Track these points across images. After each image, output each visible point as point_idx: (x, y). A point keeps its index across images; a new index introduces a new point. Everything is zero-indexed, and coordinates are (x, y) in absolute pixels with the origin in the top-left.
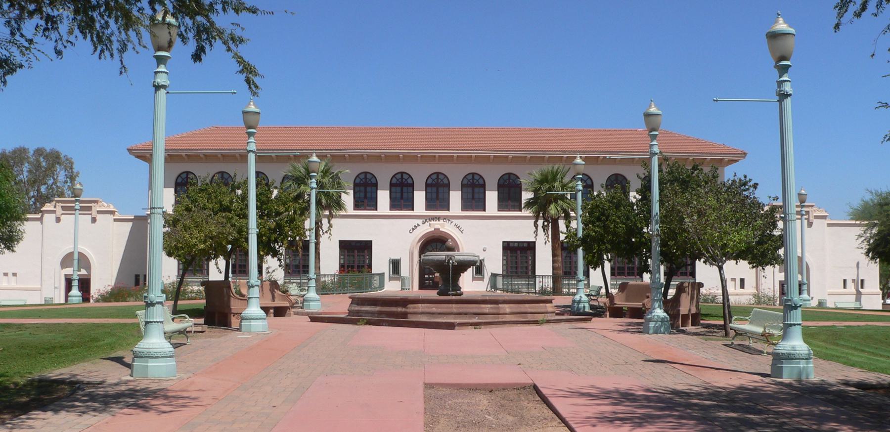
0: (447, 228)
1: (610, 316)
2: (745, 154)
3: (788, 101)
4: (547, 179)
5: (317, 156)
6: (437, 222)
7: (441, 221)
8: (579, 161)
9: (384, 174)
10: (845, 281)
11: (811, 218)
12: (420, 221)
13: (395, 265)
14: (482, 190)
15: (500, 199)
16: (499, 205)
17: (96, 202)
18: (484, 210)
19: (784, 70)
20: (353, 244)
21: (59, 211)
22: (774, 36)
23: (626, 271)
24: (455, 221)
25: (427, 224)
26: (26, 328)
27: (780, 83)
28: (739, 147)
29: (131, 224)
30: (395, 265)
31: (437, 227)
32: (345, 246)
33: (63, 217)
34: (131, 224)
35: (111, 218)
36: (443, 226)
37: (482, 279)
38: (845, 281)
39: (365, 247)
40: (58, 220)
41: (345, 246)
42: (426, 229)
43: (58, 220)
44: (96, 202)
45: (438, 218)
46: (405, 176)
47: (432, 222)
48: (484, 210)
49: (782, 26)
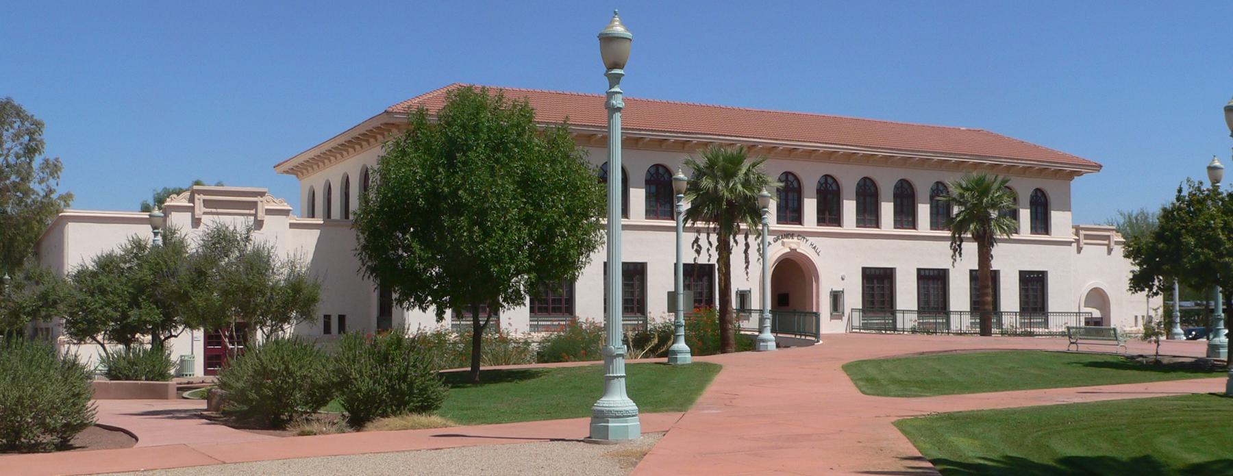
0: (803, 247)
2: (1101, 166)
3: (618, 116)
4: (981, 188)
11: (261, 215)
13: (836, 297)
15: (779, 209)
16: (895, 221)
17: (262, 194)
18: (878, 226)
19: (615, 80)
21: (200, 209)
22: (608, 40)
24: (811, 239)
27: (611, 95)
29: (317, 233)
30: (836, 297)
31: (794, 246)
34: (317, 233)
35: (286, 221)
36: (798, 244)
37: (840, 317)
40: (1079, 250)
42: (776, 251)
43: (1079, 250)
44: (262, 194)
48: (878, 226)
49: (619, 29)
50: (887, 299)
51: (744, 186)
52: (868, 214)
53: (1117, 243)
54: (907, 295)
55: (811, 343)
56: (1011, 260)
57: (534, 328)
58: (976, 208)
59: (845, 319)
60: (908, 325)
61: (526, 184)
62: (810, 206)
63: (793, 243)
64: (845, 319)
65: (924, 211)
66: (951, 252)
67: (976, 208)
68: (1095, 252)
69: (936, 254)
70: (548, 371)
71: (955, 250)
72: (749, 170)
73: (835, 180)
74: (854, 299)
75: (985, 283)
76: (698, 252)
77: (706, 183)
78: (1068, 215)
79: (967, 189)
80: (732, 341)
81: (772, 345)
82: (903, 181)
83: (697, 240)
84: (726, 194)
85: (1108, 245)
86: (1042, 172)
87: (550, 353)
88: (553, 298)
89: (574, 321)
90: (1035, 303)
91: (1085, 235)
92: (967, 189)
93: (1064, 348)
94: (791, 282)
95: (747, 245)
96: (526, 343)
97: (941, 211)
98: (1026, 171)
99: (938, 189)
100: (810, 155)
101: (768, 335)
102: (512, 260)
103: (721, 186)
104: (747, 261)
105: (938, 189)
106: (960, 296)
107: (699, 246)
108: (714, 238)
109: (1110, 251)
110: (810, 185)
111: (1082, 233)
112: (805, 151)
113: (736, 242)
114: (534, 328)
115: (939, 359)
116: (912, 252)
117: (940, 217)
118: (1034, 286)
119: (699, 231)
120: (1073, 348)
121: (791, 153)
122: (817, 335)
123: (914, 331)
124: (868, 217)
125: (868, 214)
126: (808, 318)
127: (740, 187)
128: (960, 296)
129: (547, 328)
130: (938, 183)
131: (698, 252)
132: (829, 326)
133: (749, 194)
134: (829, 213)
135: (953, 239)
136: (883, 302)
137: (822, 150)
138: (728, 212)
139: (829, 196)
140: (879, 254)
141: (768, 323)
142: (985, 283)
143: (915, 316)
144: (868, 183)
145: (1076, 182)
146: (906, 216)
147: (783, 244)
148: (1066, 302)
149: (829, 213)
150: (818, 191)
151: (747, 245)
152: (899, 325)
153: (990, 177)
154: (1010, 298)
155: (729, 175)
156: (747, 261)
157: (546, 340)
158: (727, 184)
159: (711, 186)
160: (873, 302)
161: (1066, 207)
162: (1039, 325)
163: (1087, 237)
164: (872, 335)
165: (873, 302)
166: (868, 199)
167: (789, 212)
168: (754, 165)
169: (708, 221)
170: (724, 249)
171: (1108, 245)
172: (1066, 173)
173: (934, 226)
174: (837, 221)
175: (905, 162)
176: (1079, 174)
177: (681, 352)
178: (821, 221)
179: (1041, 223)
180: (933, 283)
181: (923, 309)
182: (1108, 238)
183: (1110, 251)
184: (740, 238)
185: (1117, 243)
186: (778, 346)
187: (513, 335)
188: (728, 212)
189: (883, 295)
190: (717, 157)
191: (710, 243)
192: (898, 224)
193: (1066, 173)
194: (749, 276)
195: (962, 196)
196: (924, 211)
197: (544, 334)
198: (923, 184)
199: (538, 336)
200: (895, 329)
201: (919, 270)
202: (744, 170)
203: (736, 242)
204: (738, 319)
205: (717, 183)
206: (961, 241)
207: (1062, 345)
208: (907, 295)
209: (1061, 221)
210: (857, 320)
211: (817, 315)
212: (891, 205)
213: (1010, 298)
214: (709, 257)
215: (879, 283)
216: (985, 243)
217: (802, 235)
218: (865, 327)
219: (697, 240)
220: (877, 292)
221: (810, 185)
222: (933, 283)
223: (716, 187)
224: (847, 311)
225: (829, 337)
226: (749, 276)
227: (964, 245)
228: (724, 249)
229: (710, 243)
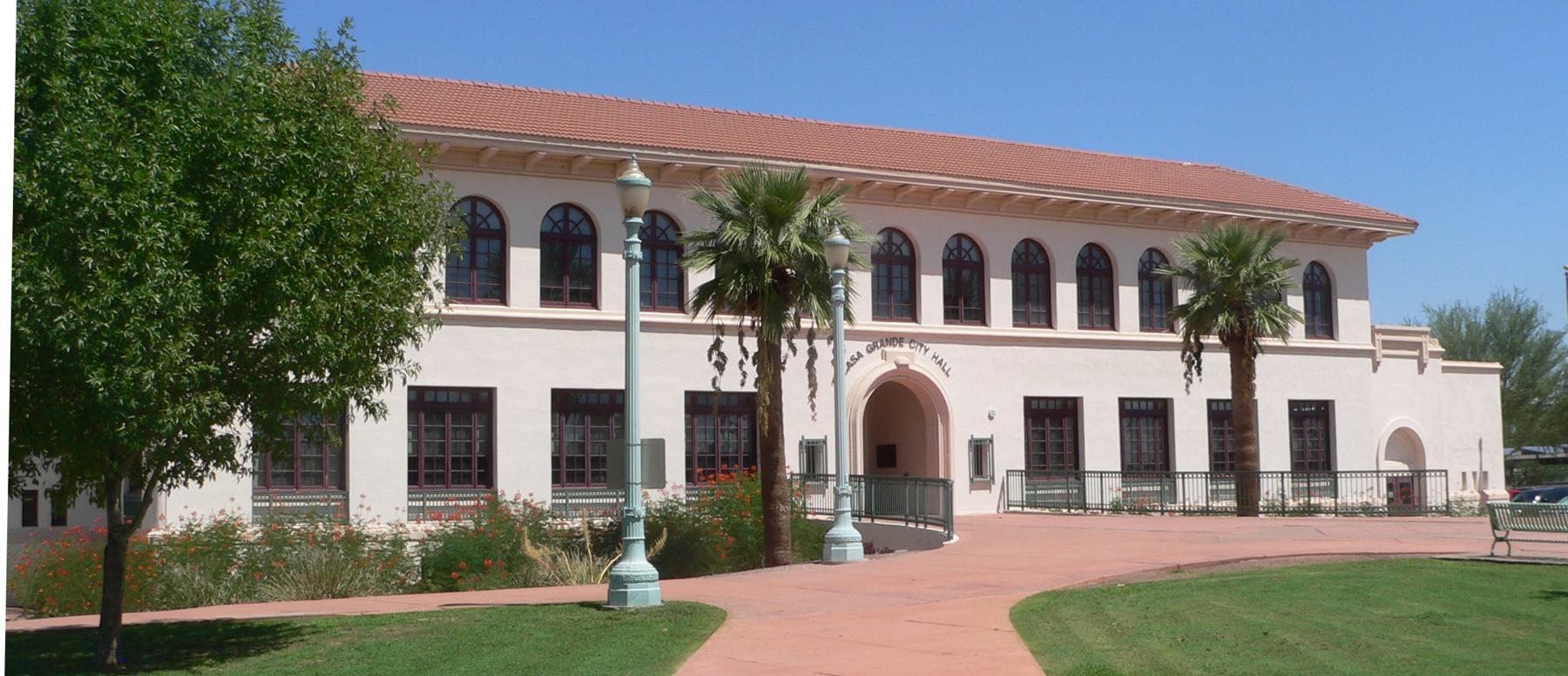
0: (920, 362)
1: (11, 636)
2: (1416, 224)
5: (643, 167)
6: (897, 349)
7: (906, 346)
8: (636, 175)
9: (525, 205)
10: (1464, 474)
11: (1426, 356)
12: (861, 346)
13: (980, 451)
14: (495, 245)
20: (593, 399)
23: (589, 469)
24: (934, 348)
25: (877, 352)
26: (315, 630)
28: (1404, 213)
30: (980, 451)
31: (903, 360)
32: (566, 403)
33: (1385, 362)
36: (911, 356)
37: (987, 486)
38: (1464, 474)
39: (475, 406)
40: (1376, 366)
41: (566, 403)
42: (871, 369)
43: (1376, 366)
45: (897, 339)
46: (482, 210)
47: (888, 349)
50: (1069, 452)
51: (803, 238)
52: (1034, 302)
53: (1433, 354)
54: (1102, 444)
55: (935, 542)
56: (1282, 379)
57: (416, 514)
58: (1231, 288)
59: (996, 488)
60: (1108, 499)
61: (201, 167)
62: (932, 288)
63: (902, 354)
64: (996, 488)
65: (1128, 298)
66: (1184, 367)
67: (1231, 288)
68: (1399, 369)
69: (1154, 370)
70: (344, 622)
71: (1190, 364)
72: (814, 211)
73: (974, 244)
74: (1010, 453)
75: (1232, 423)
76: (720, 366)
77: (734, 234)
78: (1364, 305)
79: (1210, 254)
80: (786, 536)
81: (855, 550)
82: (1091, 246)
83: (717, 345)
84: (772, 255)
85: (1419, 359)
86: (1322, 233)
87: (447, 567)
88: (303, 452)
89: (494, 502)
90: (1316, 455)
91: (1395, 342)
92: (1210, 254)
93: (1483, 551)
94: (899, 426)
95: (813, 353)
96: (398, 543)
97: (1157, 298)
98: (1299, 230)
99: (1153, 260)
100: (930, 197)
101: (846, 529)
102: (150, 359)
103: (762, 241)
104: (813, 384)
105: (1153, 260)
106: (1192, 445)
107: (721, 355)
108: (752, 344)
109: (1422, 367)
110: (931, 252)
111: (1380, 337)
112: (920, 190)
113: (793, 348)
114: (416, 514)
115: (1225, 585)
116: (1112, 368)
117: (1157, 310)
118: (1313, 421)
119: (721, 329)
120: (1501, 549)
121: (896, 193)
122: (947, 522)
123: (1116, 509)
124: (1033, 309)
125: (1034, 302)
126: (929, 490)
127: (796, 241)
128: (1192, 445)
129: (436, 515)
130: (1151, 251)
131: (720, 366)
132: (968, 503)
133: (813, 253)
134: (966, 301)
135: (1186, 346)
136: (1061, 458)
137: (951, 188)
138: (772, 289)
139: (966, 273)
140: (1053, 373)
141: (847, 505)
142: (1232, 423)
143: (1117, 482)
144: (1033, 249)
145: (1376, 252)
146: (1098, 305)
147: (884, 356)
148: (1359, 448)
149: (966, 301)
150: (947, 264)
151: (813, 353)
152: (1092, 497)
153: (1249, 233)
154: (1274, 447)
155: (776, 220)
156: (813, 384)
157: (431, 536)
158: (775, 237)
159: (743, 238)
160: (1043, 459)
161: (1361, 293)
162: (1322, 492)
163: (1386, 345)
164: (1044, 520)
165: (1043, 459)
166: (1033, 278)
167: (896, 297)
168: (824, 204)
169: (739, 310)
170: (769, 361)
171: (1419, 359)
172: (1360, 235)
173: (1147, 324)
174: (981, 317)
175: (1096, 213)
176: (1380, 237)
177: (636, 581)
178: (951, 315)
179: (1322, 320)
180: (1147, 421)
181: (1130, 470)
182: (1419, 346)
183: (1422, 367)
184: (801, 344)
185: (1433, 354)
186: (869, 549)
187: (372, 529)
188: (772, 289)
189: (1061, 446)
190: (755, 184)
191: (744, 350)
192: (1085, 321)
193: (1360, 235)
194: (819, 410)
195: (1201, 266)
196: (1128, 298)
197: (432, 526)
198: (1126, 253)
199: (419, 529)
200: (1084, 506)
201: (1122, 401)
202: (806, 212)
203: (793, 348)
204: (804, 491)
205: (753, 232)
206: (1201, 347)
207: (1474, 539)
208: (1102, 444)
209: (1352, 315)
210: (1017, 491)
211: (947, 485)
212: (1073, 287)
213: (1274, 447)
214: (739, 379)
215: (1053, 423)
216: (1243, 351)
217: (918, 340)
218: (1031, 502)
219: (717, 345)
220: (1051, 439)
221: (931, 252)
222: (1147, 421)
223: (750, 240)
224: (999, 475)
225: (974, 523)
226: (819, 410)
227: (1203, 355)
228: (769, 361)
229: (744, 350)
